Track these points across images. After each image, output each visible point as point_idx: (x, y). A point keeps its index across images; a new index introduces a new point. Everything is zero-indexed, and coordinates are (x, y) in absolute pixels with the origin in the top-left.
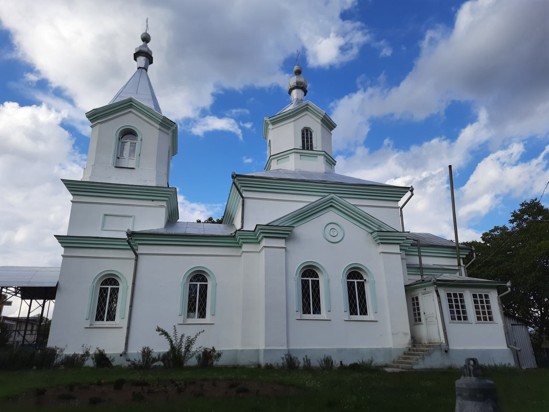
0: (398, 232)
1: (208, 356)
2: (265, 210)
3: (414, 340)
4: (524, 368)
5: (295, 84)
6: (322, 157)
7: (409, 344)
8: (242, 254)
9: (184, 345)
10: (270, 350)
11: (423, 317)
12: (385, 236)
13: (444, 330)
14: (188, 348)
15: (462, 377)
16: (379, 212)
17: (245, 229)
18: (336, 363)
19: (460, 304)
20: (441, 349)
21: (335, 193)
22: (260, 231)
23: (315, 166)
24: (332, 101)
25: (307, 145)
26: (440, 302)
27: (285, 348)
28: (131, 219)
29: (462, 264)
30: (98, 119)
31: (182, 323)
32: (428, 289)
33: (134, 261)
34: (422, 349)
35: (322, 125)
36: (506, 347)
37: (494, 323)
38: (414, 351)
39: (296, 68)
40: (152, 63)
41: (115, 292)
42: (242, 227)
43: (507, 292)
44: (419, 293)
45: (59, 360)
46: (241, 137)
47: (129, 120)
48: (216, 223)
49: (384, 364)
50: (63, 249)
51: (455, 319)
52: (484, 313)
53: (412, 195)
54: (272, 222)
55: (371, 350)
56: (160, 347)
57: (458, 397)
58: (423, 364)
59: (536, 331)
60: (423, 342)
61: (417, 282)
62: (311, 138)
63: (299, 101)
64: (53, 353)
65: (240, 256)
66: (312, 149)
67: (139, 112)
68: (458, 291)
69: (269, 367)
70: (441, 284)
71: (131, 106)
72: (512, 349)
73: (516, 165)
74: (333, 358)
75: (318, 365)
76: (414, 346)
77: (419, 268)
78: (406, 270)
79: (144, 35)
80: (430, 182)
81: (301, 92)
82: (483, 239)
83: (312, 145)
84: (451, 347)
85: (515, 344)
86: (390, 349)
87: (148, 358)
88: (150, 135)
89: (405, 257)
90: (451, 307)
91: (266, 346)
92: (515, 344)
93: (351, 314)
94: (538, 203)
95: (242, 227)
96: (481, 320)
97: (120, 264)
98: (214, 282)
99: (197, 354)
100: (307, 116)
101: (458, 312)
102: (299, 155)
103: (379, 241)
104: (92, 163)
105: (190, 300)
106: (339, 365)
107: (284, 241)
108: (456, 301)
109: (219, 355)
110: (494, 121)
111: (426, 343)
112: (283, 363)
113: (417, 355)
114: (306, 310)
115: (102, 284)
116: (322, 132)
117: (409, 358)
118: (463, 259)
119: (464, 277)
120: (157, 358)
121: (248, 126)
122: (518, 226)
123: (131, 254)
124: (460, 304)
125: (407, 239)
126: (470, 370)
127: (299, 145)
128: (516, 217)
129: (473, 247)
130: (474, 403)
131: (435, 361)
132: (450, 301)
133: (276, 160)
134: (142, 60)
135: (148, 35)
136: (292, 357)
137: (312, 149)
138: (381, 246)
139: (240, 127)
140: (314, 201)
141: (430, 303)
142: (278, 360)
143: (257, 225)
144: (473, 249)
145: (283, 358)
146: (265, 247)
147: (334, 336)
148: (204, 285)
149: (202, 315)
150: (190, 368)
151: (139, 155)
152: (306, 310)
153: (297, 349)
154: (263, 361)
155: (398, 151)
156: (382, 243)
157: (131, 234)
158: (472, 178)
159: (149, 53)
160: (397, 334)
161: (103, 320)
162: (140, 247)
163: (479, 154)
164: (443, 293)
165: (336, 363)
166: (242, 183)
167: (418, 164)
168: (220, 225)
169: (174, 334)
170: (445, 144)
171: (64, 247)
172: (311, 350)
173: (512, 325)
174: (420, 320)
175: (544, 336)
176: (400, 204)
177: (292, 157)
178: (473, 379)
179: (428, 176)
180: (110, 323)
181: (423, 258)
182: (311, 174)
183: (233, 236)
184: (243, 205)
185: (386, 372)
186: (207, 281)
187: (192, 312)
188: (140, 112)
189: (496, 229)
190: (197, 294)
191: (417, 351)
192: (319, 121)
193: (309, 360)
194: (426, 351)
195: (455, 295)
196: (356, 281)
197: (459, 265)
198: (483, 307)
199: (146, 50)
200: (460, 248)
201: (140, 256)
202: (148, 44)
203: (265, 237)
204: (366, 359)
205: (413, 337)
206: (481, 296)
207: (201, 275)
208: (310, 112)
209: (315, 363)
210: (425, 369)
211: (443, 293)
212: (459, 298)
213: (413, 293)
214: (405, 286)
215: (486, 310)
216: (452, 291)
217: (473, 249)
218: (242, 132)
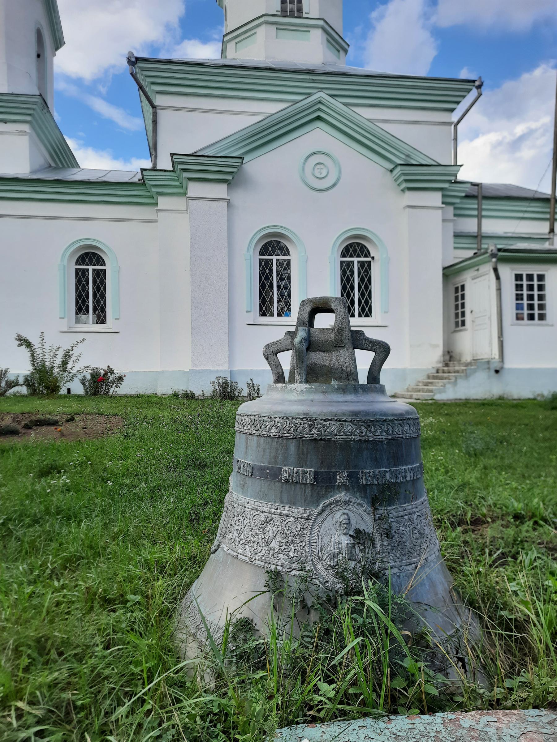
0: (440, 165)
6: (319, 32)
7: (439, 362)
11: (468, 318)
12: (419, 175)
13: (499, 338)
20: (489, 368)
26: (499, 289)
31: (66, 330)
34: (457, 368)
37: (547, 325)
42: (155, 164)
51: (522, 319)
53: (480, 95)
58: (449, 392)
68: (535, 270)
70: (507, 256)
76: (447, 365)
77: (476, 237)
78: (451, 239)
84: (508, 365)
90: (519, 297)
93: (263, 314)
95: (155, 164)
102: (273, 28)
103: (404, 185)
107: (224, 187)
108: (531, 288)
109: (120, 379)
113: (446, 378)
131: (476, 387)
132: (519, 287)
138: (408, 194)
141: (483, 291)
145: (213, 383)
148: (101, 270)
149: (101, 319)
153: (247, 371)
156: (410, 189)
164: (508, 273)
169: (40, 345)
177: (262, 31)
191: (449, 372)
193: (258, 386)
195: (530, 277)
207: (94, 254)
216: (525, 270)
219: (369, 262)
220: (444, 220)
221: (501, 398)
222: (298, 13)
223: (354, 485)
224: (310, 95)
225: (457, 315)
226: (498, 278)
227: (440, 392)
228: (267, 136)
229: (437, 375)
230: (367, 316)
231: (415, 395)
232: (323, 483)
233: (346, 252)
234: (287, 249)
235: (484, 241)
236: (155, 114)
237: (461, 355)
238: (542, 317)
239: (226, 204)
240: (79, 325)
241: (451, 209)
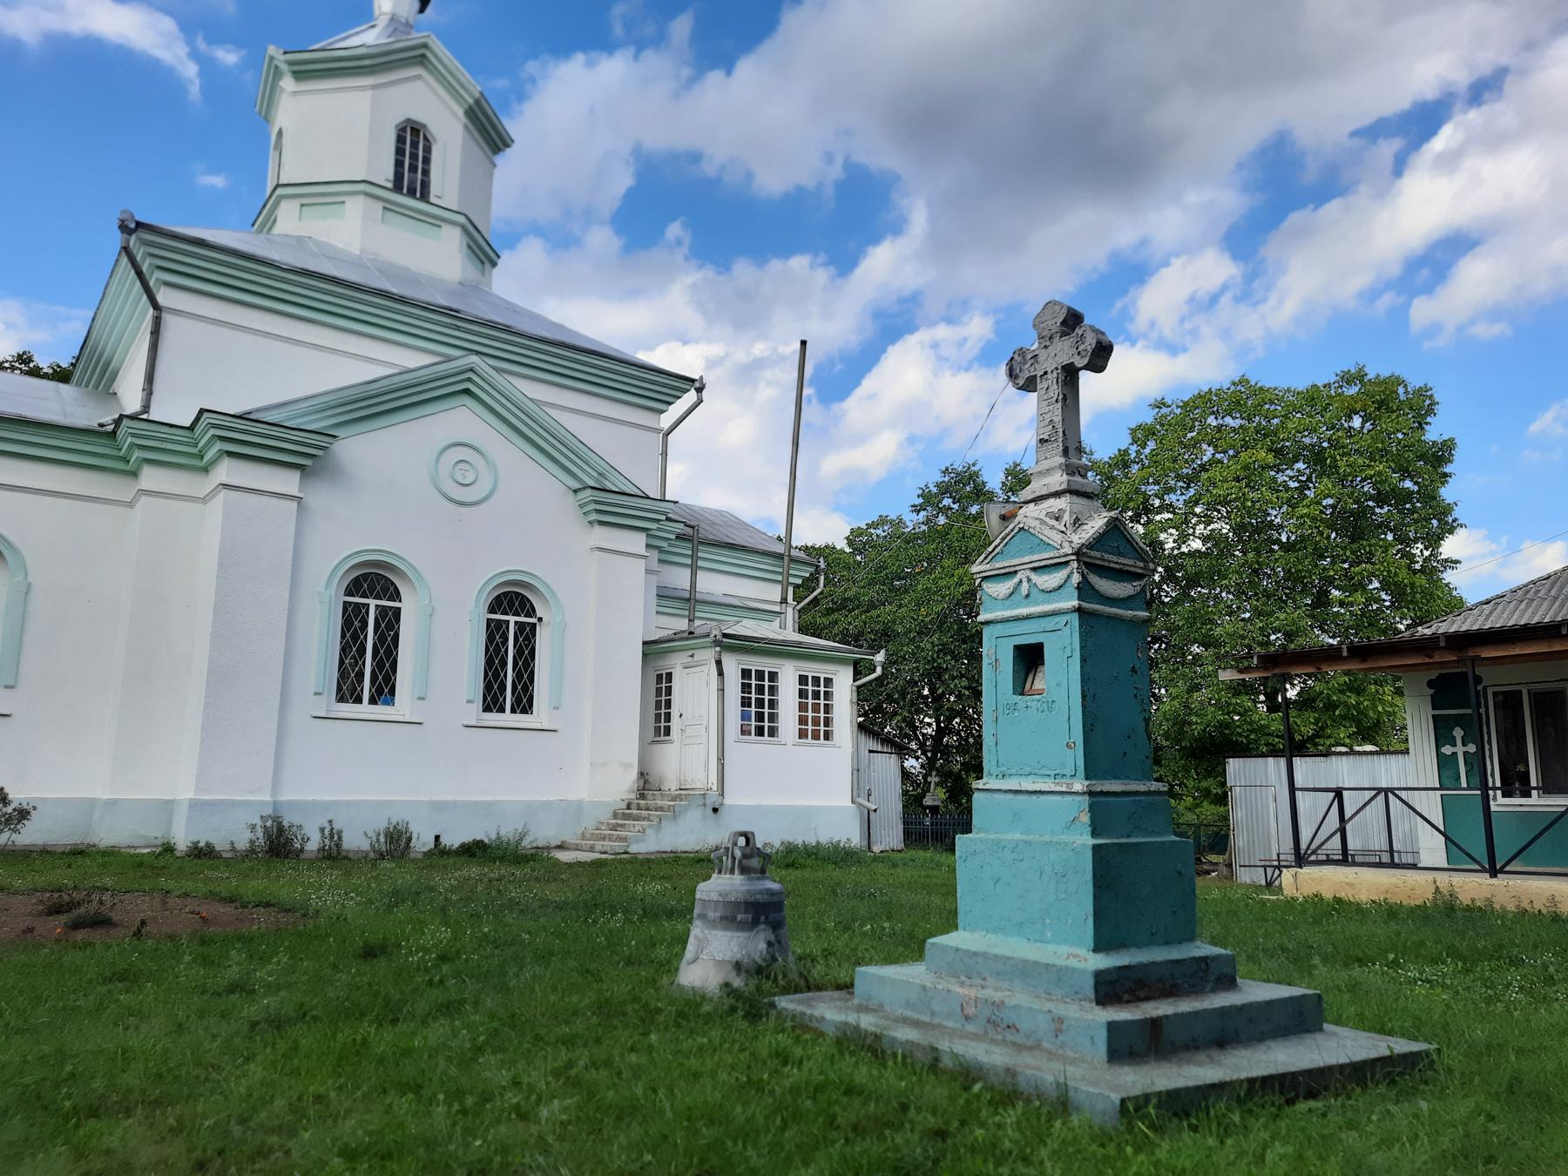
2: (229, 362)
4: (876, 849)
8: (213, 493)
11: (675, 724)
12: (612, 505)
15: (715, 875)
16: (604, 431)
17: (154, 415)
18: (422, 841)
19: (766, 697)
21: (481, 354)
22: (212, 432)
23: (428, 257)
24: (536, 58)
26: (722, 690)
29: (790, 599)
34: (660, 803)
35: (466, 126)
37: (834, 746)
46: (195, 90)
48: (45, 376)
49: (553, 843)
52: (816, 722)
53: (700, 401)
57: (697, 923)
58: (650, 841)
59: (922, 766)
60: (665, 787)
61: (677, 636)
62: (427, 161)
65: (130, 505)
66: (425, 197)
69: (202, 854)
73: (967, 369)
74: (413, 828)
75: (365, 845)
76: (642, 797)
77: (689, 600)
78: (654, 600)
80: (768, 374)
82: (850, 542)
83: (425, 186)
84: (729, 800)
86: (579, 806)
89: (655, 566)
90: (745, 703)
94: (976, 474)
98: (20, 578)
100: (419, 83)
101: (760, 717)
102: (379, 206)
103: (594, 516)
107: (295, 476)
108: (760, 690)
109: (23, 814)
110: (940, 246)
112: (252, 842)
118: (796, 587)
121: (228, 57)
122: (928, 521)
125: (668, 519)
126: (734, 858)
127: (386, 173)
128: (928, 500)
130: (729, 934)
132: (746, 688)
133: (296, 203)
136: (285, 824)
137: (425, 197)
138: (598, 529)
139: (194, 55)
140: (412, 365)
141: (700, 690)
142: (235, 832)
143: (202, 411)
144: (822, 565)
146: (225, 486)
147: (425, 770)
152: (348, 691)
153: (306, 803)
155: (701, 267)
156: (602, 523)
158: (869, 383)
163: (892, 323)
164: (733, 665)
165: (422, 841)
166: (157, 255)
167: (743, 315)
168: (61, 386)
170: (822, 276)
172: (349, 804)
174: (668, 731)
175: (934, 779)
176: (666, 420)
178: (738, 878)
179: (766, 354)
182: (415, 279)
184: (156, 333)
189: (883, 520)
192: (460, 112)
193: (340, 833)
197: (784, 601)
198: (816, 708)
200: (793, 560)
203: (231, 454)
204: (508, 831)
205: (642, 774)
208: (431, 73)
209: (355, 840)
211: (733, 665)
212: (767, 683)
213: (661, 663)
214: (644, 643)
216: (756, 663)
217: (822, 565)
218: (201, 74)
220: (647, 572)
222: (422, 191)
223: (767, 922)
224: (450, 359)
225: (658, 717)
226: (721, 673)
227: (637, 842)
229: (628, 813)
230: (524, 711)
231: (599, 845)
232: (755, 923)
233: (355, 587)
234: (396, 589)
236: (157, 322)
238: (773, 732)
239: (295, 504)
241: (655, 555)
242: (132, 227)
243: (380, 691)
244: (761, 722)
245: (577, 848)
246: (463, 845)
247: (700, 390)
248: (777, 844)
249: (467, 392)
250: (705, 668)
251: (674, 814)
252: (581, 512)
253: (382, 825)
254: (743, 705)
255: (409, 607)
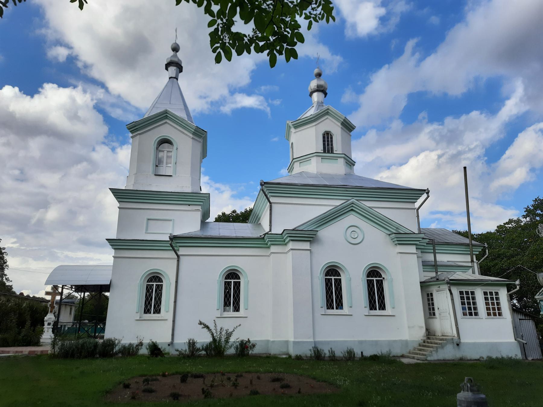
0: (415, 234)
1: (244, 347)
3: (429, 332)
4: (530, 358)
5: (316, 87)
7: (424, 336)
9: (223, 339)
10: (298, 342)
11: (436, 311)
14: (227, 341)
15: (462, 392)
19: (471, 301)
20: (453, 342)
22: (287, 235)
23: (335, 169)
25: (328, 149)
26: (452, 300)
27: (312, 340)
28: (171, 223)
29: (475, 260)
30: (138, 130)
31: (219, 316)
32: (442, 287)
33: (176, 261)
36: (513, 340)
38: (428, 343)
39: (316, 71)
40: (182, 71)
41: (159, 288)
42: (270, 230)
43: (516, 290)
44: (434, 290)
45: (117, 349)
47: (166, 130)
49: (399, 355)
50: (113, 251)
51: (466, 315)
52: (494, 309)
53: (428, 197)
54: (298, 227)
55: (389, 342)
56: (203, 338)
62: (332, 141)
63: (320, 104)
64: (111, 344)
66: (332, 152)
67: (173, 122)
68: (469, 289)
69: (299, 358)
71: (166, 117)
72: (519, 342)
75: (342, 355)
76: (429, 338)
77: (434, 266)
78: (422, 267)
79: (174, 46)
81: (321, 95)
83: (332, 148)
84: (462, 341)
85: (522, 337)
87: (193, 347)
88: (185, 144)
89: (420, 254)
90: (463, 303)
91: (295, 338)
92: (522, 337)
93: (371, 309)
95: (270, 230)
96: (491, 315)
97: (165, 263)
99: (235, 345)
100: (327, 120)
101: (470, 309)
102: (320, 158)
103: (397, 242)
104: (135, 172)
105: (226, 296)
106: (361, 356)
107: (308, 243)
108: (468, 298)
109: (254, 346)
111: (440, 335)
114: (330, 306)
115: (148, 281)
116: (342, 136)
117: (423, 350)
118: (476, 255)
119: (477, 276)
120: (201, 348)
123: (172, 254)
124: (471, 301)
129: (486, 244)
131: (448, 353)
132: (462, 298)
133: (298, 163)
134: (173, 70)
135: (178, 45)
137: (332, 152)
138: (398, 246)
140: (338, 204)
141: (443, 299)
142: (306, 351)
144: (486, 245)
145: (310, 350)
146: (292, 249)
147: (353, 330)
149: (237, 309)
150: (230, 357)
151: (176, 163)
152: (330, 306)
154: (293, 352)
156: (399, 244)
157: (173, 238)
159: (179, 63)
160: (413, 327)
161: (150, 313)
162: (181, 249)
164: (456, 291)
166: (270, 189)
171: (115, 249)
172: (335, 341)
173: (520, 319)
174: (434, 314)
176: (417, 205)
177: (314, 160)
180: (156, 316)
181: (437, 255)
183: (262, 238)
184: (271, 210)
185: (403, 364)
186: (240, 279)
187: (228, 306)
188: (175, 123)
189: (510, 221)
190: (232, 291)
191: (431, 343)
192: (339, 124)
194: (440, 344)
195: (467, 293)
196: (375, 279)
197: (472, 261)
198: (493, 304)
199: (175, 59)
201: (181, 257)
202: (177, 53)
203: (292, 240)
206: (491, 293)
207: (158, 277)
210: (438, 360)
211: (456, 291)
212: (470, 296)
214: (420, 282)
215: (496, 306)
216: (464, 289)
217: (486, 245)
219: (382, 280)
220: (418, 257)
221: (461, 359)
224: (348, 200)
226: (451, 294)
227: (430, 356)
228: (326, 219)
235: (438, 268)
236: (271, 207)
237: (435, 332)
238: (476, 314)
240: (225, 313)
241: (420, 251)
242: (263, 184)
243: (338, 305)
244: (470, 310)
245: (408, 357)
246: (371, 356)
247: (428, 193)
248: (485, 358)
249: (352, 210)
250: (445, 291)
251: (442, 346)
252: (392, 241)
253: (346, 349)
254: (462, 305)
255: (164, 284)
